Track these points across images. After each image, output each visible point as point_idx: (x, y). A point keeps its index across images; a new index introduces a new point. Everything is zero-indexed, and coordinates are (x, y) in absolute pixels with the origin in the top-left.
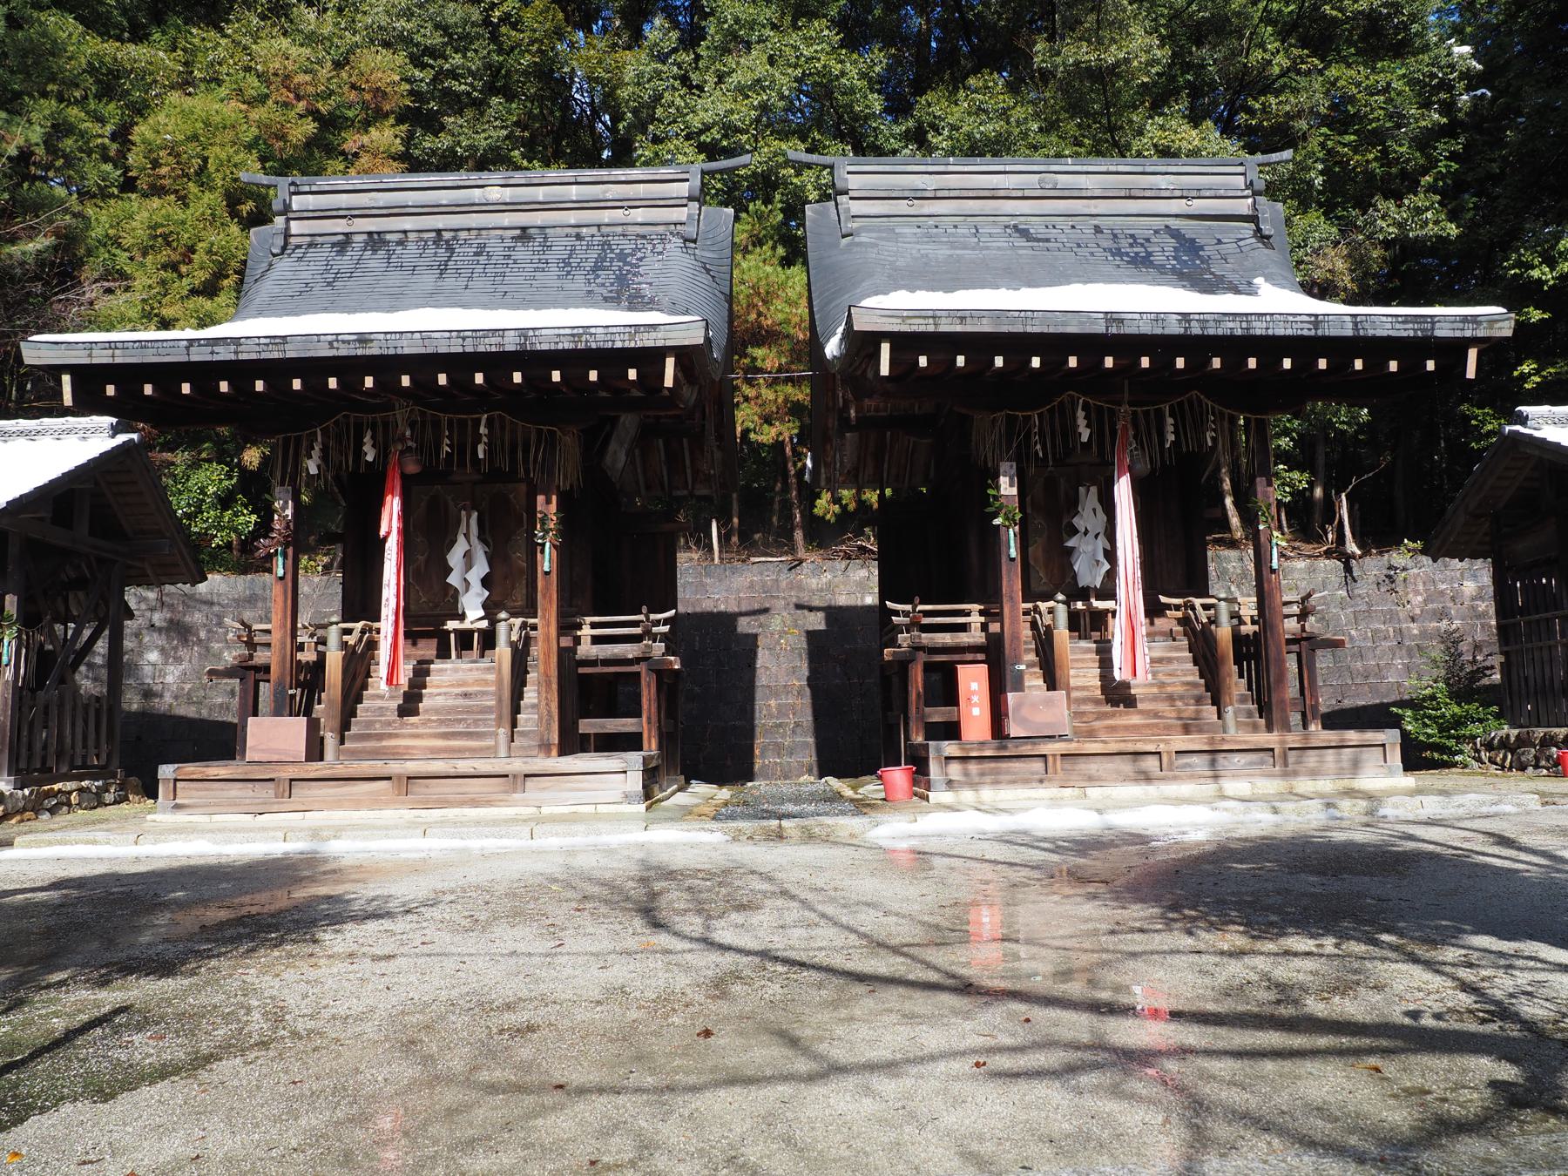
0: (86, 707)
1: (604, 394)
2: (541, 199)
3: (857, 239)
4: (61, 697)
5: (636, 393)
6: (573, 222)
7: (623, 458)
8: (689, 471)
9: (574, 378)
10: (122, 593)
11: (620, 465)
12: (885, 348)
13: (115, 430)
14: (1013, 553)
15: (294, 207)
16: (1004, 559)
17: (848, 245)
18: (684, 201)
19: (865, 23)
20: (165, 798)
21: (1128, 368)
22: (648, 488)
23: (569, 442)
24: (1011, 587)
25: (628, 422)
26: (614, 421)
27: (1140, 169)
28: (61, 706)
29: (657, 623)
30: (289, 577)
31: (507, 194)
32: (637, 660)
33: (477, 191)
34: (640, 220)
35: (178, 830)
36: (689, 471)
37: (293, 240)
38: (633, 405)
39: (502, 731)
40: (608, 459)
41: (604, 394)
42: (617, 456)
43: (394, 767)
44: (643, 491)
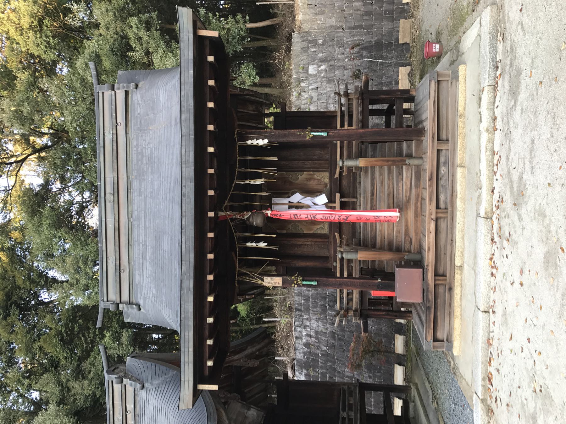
34: (133, 406)
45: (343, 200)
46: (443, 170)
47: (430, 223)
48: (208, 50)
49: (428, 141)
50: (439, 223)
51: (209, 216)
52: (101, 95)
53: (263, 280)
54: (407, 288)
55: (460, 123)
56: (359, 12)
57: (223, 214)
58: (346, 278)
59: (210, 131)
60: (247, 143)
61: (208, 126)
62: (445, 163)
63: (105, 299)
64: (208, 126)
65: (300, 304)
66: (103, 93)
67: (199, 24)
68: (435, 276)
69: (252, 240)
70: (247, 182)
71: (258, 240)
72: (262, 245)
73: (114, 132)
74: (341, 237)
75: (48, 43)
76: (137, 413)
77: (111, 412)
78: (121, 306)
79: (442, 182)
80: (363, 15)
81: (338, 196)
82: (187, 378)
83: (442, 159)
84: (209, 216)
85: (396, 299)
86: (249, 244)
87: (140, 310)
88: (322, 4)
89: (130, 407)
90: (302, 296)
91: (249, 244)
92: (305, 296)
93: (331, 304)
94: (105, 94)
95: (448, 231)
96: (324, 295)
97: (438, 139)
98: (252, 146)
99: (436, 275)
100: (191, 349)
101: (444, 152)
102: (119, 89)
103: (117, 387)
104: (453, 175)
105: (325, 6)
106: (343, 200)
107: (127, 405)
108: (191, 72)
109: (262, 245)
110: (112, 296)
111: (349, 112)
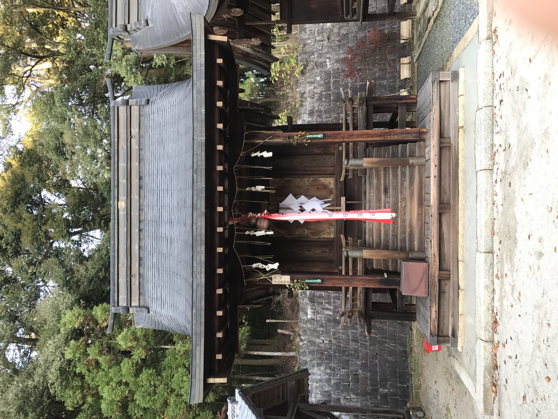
2: (125, 181)
3: (149, 17)
5: (227, 167)
6: (137, 164)
10: (313, 405)
12: (211, 380)
13: (234, 401)
14: (319, 281)
15: (125, 305)
17: (152, 22)
18: (129, 107)
19: (30, 197)
21: (224, 136)
27: (116, 190)
30: (321, 276)
31: (123, 198)
34: (137, 130)
35: (411, 214)
37: (142, 304)
45: (348, 202)
48: (217, 54)
49: (433, 142)
51: (218, 272)
54: (413, 281)
58: (351, 276)
59: (219, 150)
60: (252, 267)
61: (218, 82)
64: (218, 82)
66: (118, 107)
68: (439, 270)
74: (346, 239)
76: (141, 134)
77: (116, 140)
81: (343, 199)
84: (218, 272)
85: (399, 300)
87: (149, 312)
89: (135, 131)
94: (119, 108)
99: (441, 269)
103: (123, 110)
106: (348, 202)
107: (132, 130)
108: (203, 110)
110: (123, 303)
111: (353, 124)
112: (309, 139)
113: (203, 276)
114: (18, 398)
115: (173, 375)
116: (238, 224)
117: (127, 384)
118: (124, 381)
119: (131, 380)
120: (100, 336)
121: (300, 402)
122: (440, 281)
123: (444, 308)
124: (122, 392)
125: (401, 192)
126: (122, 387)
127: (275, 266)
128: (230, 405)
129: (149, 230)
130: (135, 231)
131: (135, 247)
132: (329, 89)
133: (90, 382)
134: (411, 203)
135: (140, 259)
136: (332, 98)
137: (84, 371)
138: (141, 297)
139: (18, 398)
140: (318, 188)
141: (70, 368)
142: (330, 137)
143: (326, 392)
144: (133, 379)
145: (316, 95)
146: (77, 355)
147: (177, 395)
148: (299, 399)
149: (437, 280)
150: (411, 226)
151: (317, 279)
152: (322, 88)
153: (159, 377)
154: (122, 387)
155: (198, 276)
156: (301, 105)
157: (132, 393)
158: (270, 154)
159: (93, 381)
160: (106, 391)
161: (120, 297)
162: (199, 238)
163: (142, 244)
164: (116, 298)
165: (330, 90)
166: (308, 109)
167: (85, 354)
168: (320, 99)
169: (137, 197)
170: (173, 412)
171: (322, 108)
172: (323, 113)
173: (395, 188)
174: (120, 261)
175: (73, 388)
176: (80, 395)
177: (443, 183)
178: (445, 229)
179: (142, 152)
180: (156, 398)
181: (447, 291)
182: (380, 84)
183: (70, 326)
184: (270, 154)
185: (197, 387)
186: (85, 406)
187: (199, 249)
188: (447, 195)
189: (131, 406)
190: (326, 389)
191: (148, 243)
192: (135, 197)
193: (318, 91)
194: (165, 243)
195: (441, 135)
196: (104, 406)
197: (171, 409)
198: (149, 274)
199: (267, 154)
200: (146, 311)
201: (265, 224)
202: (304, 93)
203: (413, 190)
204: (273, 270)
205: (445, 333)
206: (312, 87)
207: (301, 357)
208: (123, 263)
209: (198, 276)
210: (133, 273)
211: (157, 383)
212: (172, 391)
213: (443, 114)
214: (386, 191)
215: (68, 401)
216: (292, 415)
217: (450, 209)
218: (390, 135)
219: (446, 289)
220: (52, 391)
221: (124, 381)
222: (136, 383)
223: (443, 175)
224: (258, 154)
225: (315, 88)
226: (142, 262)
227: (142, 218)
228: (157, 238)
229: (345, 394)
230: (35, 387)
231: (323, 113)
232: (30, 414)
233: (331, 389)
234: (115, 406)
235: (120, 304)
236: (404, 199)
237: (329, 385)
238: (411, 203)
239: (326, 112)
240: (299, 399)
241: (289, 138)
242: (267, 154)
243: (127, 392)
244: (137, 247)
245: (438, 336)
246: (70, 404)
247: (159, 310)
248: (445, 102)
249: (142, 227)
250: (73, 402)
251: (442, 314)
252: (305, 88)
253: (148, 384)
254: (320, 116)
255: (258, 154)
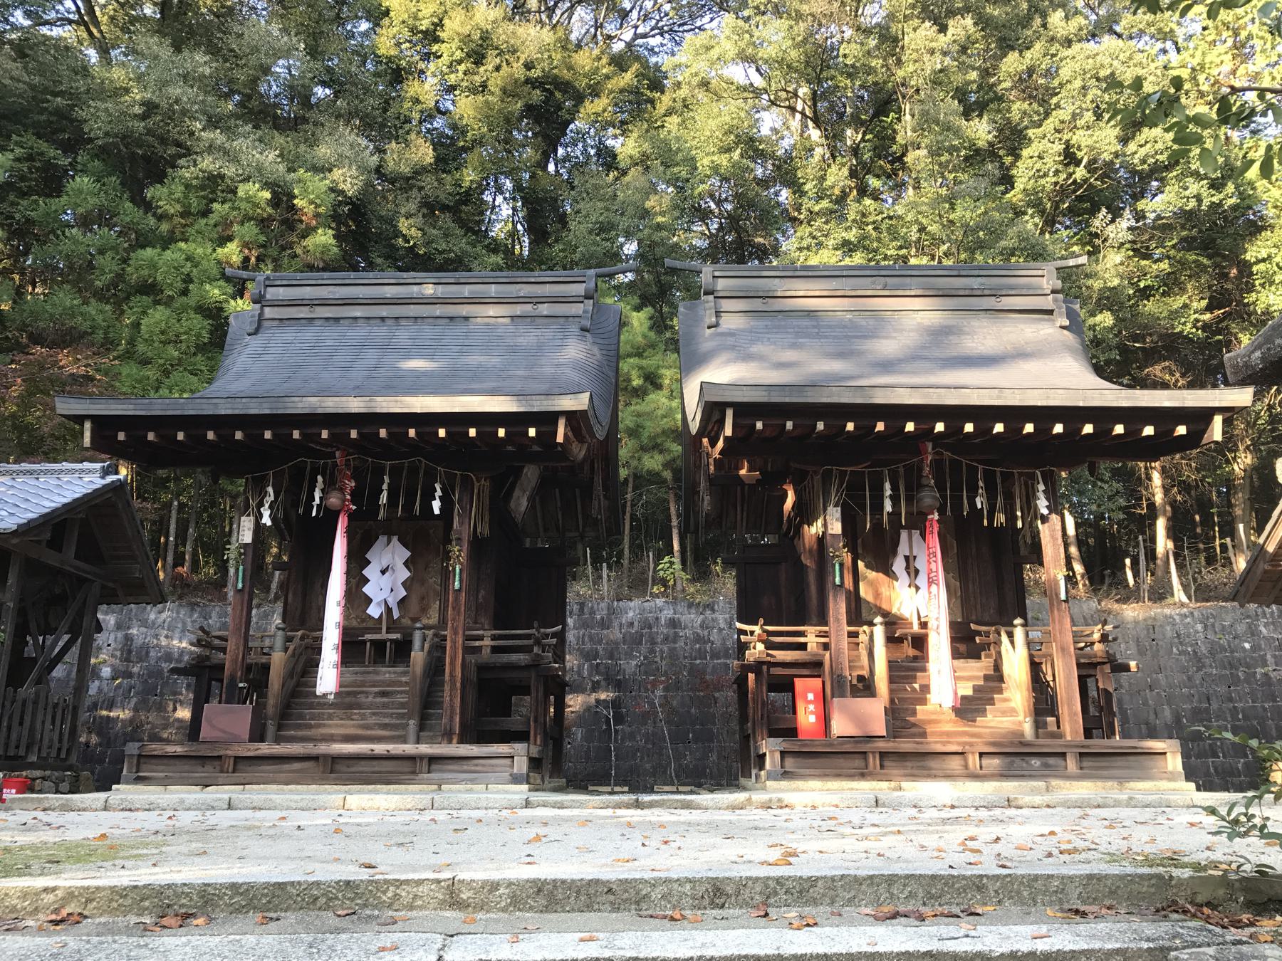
0: (56, 706)
1: (510, 448)
2: (466, 295)
4: (37, 694)
5: (535, 448)
7: (525, 503)
8: (580, 516)
9: (487, 436)
11: (523, 509)
12: (729, 414)
15: (268, 297)
16: (830, 585)
17: (711, 335)
20: (129, 771)
22: (546, 530)
23: (482, 485)
24: (837, 610)
25: (531, 474)
26: (518, 472)
28: (35, 703)
29: (547, 636)
30: (247, 590)
31: (441, 291)
32: (527, 667)
33: (415, 288)
34: (545, 313)
36: (580, 516)
37: (266, 323)
38: (534, 458)
39: (412, 722)
40: (512, 504)
41: (510, 448)
42: (521, 503)
43: (323, 748)
44: (542, 534)
46: (1036, 762)
47: (959, 743)
50: (957, 757)
52: (1040, 273)
53: (836, 506)
55: (1110, 783)
56: (1152, 717)
57: (930, 449)
62: (1046, 766)
63: (717, 274)
65: (593, 612)
67: (1229, 414)
68: (236, 758)
69: (895, 488)
70: (981, 484)
71: (895, 499)
72: (888, 506)
73: (986, 292)
75: (1045, 175)
78: (711, 297)
79: (1017, 760)
80: (1147, 724)
82: (113, 407)
83: (1051, 761)
86: (887, 486)
88: (1158, 651)
89: (544, 309)
90: (609, 615)
91: (887, 486)
92: (610, 621)
93: (602, 668)
95: (823, 856)
96: (616, 656)
97: (1081, 754)
98: (1035, 491)
99: (237, 759)
100: (787, 400)
101: (1063, 763)
102: (1055, 300)
103: (579, 289)
104: (1031, 777)
105: (1155, 656)
109: (888, 506)
112: (454, 569)
113: (229, 412)
114: (171, 105)
115: (196, 375)
116: (335, 465)
117: (185, 292)
118: (191, 287)
119: (192, 300)
120: (281, 242)
121: (103, 587)
122: (220, 757)
123: (180, 766)
124: (171, 285)
125: (374, 714)
126: (180, 285)
127: (266, 520)
128: (98, 466)
129: (381, 332)
130: (384, 311)
131: (358, 312)
132: (715, 655)
133: (196, 227)
134: (354, 726)
135: (337, 319)
136: (698, 662)
137: (213, 218)
138: (276, 323)
139: (171, 105)
140: (423, 598)
141: (223, 191)
142: (457, 599)
143: (148, 653)
144: (192, 303)
145: (706, 633)
146: (243, 205)
147: (159, 382)
148: (111, 585)
149: (222, 753)
150: (319, 726)
151: (243, 582)
152: (718, 643)
153: (192, 349)
154: (180, 285)
155: (228, 406)
156: (690, 605)
157: (169, 302)
158: (437, 511)
159: (198, 232)
160: (174, 256)
161: (281, 289)
162: (280, 405)
163: (361, 323)
164: (278, 283)
165: (712, 658)
166: (683, 618)
167: (247, 218)
168: (698, 639)
169: (438, 313)
170: (128, 375)
171: (681, 643)
172: (672, 645)
173: (385, 706)
174: (338, 288)
175: (186, 197)
176: (172, 211)
177: (363, 763)
178: (297, 766)
179: (411, 322)
180: (156, 344)
181: (206, 768)
182: (711, 751)
183: (296, 192)
184: (437, 511)
185: (78, 406)
186: (152, 221)
187: (265, 405)
188: (345, 769)
189: (146, 300)
190: (152, 654)
191: (361, 332)
192: (438, 310)
193: (715, 636)
194: (349, 358)
195: (433, 760)
196: (149, 252)
197: (135, 370)
198: (309, 334)
199: (436, 506)
200: (251, 329)
201: (334, 500)
202: (713, 610)
203: (371, 729)
204: (261, 515)
205: (144, 767)
206: (722, 625)
207: (217, 609)
208: (334, 293)
209: (228, 406)
210: (318, 309)
211: (184, 346)
212: (167, 373)
213: (465, 762)
214: (384, 694)
215: (165, 190)
216: (77, 568)
217: (323, 772)
218: (451, 690)
219: (209, 768)
220: (182, 162)
221: (191, 287)
222: (185, 308)
223: (375, 763)
224: (439, 493)
225: (721, 630)
226: (332, 322)
227: (403, 322)
228: (362, 346)
229: (139, 687)
230: (192, 134)
231: (672, 645)
232: (143, 124)
233: (152, 662)
234: (145, 272)
235: (269, 289)
236: (363, 717)
237: (159, 659)
238: (354, 726)
239: (672, 650)
240: (111, 585)
241: (459, 539)
242: (436, 506)
243: (170, 293)
244: (358, 314)
245: (140, 756)
246: (158, 193)
247: (248, 350)
248: (483, 765)
249: (389, 322)
250: (161, 199)
251: (172, 761)
252: (723, 612)
253: (182, 330)
254: (666, 639)
255: (439, 493)
